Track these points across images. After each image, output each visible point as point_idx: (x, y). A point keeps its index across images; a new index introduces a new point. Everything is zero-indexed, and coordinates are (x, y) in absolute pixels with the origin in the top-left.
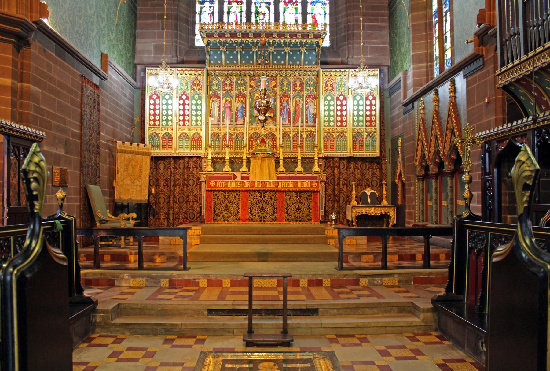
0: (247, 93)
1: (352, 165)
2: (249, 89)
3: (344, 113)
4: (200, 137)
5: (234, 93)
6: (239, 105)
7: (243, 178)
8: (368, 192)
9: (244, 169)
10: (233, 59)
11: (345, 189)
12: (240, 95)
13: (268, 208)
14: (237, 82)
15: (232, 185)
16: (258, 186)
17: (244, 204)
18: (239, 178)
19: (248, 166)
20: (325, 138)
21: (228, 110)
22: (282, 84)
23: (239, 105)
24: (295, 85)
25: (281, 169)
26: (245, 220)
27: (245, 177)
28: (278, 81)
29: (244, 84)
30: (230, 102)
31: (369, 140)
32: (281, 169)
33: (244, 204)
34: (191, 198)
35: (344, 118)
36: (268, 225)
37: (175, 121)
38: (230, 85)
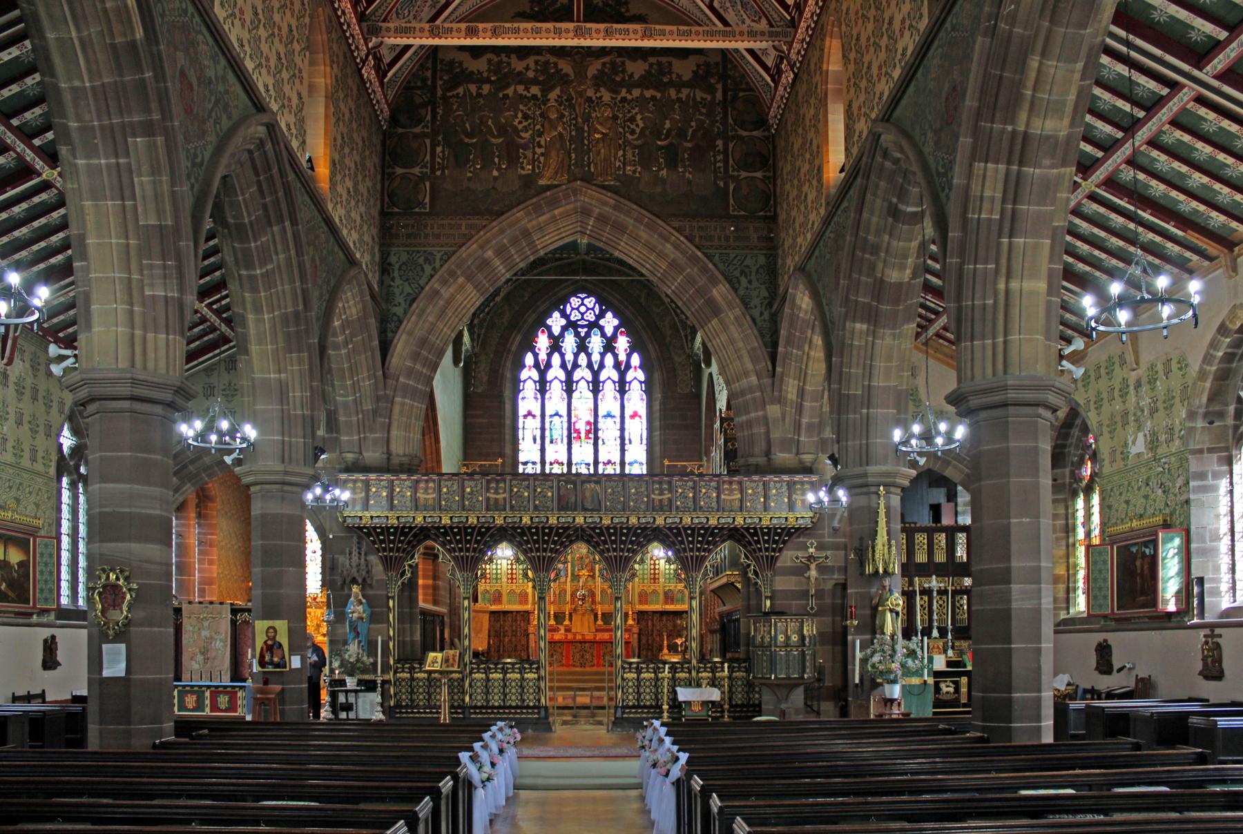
1: (664, 618)
4: (526, 594)
7: (566, 630)
8: (679, 641)
9: (567, 622)
13: (588, 656)
15: (557, 637)
16: (579, 637)
17: (568, 653)
18: (562, 631)
19: (571, 620)
20: (640, 594)
25: (600, 622)
26: (568, 666)
27: (568, 630)
31: (679, 596)
32: (600, 622)
33: (568, 653)
34: (519, 648)
36: (588, 669)
37: (504, 580)
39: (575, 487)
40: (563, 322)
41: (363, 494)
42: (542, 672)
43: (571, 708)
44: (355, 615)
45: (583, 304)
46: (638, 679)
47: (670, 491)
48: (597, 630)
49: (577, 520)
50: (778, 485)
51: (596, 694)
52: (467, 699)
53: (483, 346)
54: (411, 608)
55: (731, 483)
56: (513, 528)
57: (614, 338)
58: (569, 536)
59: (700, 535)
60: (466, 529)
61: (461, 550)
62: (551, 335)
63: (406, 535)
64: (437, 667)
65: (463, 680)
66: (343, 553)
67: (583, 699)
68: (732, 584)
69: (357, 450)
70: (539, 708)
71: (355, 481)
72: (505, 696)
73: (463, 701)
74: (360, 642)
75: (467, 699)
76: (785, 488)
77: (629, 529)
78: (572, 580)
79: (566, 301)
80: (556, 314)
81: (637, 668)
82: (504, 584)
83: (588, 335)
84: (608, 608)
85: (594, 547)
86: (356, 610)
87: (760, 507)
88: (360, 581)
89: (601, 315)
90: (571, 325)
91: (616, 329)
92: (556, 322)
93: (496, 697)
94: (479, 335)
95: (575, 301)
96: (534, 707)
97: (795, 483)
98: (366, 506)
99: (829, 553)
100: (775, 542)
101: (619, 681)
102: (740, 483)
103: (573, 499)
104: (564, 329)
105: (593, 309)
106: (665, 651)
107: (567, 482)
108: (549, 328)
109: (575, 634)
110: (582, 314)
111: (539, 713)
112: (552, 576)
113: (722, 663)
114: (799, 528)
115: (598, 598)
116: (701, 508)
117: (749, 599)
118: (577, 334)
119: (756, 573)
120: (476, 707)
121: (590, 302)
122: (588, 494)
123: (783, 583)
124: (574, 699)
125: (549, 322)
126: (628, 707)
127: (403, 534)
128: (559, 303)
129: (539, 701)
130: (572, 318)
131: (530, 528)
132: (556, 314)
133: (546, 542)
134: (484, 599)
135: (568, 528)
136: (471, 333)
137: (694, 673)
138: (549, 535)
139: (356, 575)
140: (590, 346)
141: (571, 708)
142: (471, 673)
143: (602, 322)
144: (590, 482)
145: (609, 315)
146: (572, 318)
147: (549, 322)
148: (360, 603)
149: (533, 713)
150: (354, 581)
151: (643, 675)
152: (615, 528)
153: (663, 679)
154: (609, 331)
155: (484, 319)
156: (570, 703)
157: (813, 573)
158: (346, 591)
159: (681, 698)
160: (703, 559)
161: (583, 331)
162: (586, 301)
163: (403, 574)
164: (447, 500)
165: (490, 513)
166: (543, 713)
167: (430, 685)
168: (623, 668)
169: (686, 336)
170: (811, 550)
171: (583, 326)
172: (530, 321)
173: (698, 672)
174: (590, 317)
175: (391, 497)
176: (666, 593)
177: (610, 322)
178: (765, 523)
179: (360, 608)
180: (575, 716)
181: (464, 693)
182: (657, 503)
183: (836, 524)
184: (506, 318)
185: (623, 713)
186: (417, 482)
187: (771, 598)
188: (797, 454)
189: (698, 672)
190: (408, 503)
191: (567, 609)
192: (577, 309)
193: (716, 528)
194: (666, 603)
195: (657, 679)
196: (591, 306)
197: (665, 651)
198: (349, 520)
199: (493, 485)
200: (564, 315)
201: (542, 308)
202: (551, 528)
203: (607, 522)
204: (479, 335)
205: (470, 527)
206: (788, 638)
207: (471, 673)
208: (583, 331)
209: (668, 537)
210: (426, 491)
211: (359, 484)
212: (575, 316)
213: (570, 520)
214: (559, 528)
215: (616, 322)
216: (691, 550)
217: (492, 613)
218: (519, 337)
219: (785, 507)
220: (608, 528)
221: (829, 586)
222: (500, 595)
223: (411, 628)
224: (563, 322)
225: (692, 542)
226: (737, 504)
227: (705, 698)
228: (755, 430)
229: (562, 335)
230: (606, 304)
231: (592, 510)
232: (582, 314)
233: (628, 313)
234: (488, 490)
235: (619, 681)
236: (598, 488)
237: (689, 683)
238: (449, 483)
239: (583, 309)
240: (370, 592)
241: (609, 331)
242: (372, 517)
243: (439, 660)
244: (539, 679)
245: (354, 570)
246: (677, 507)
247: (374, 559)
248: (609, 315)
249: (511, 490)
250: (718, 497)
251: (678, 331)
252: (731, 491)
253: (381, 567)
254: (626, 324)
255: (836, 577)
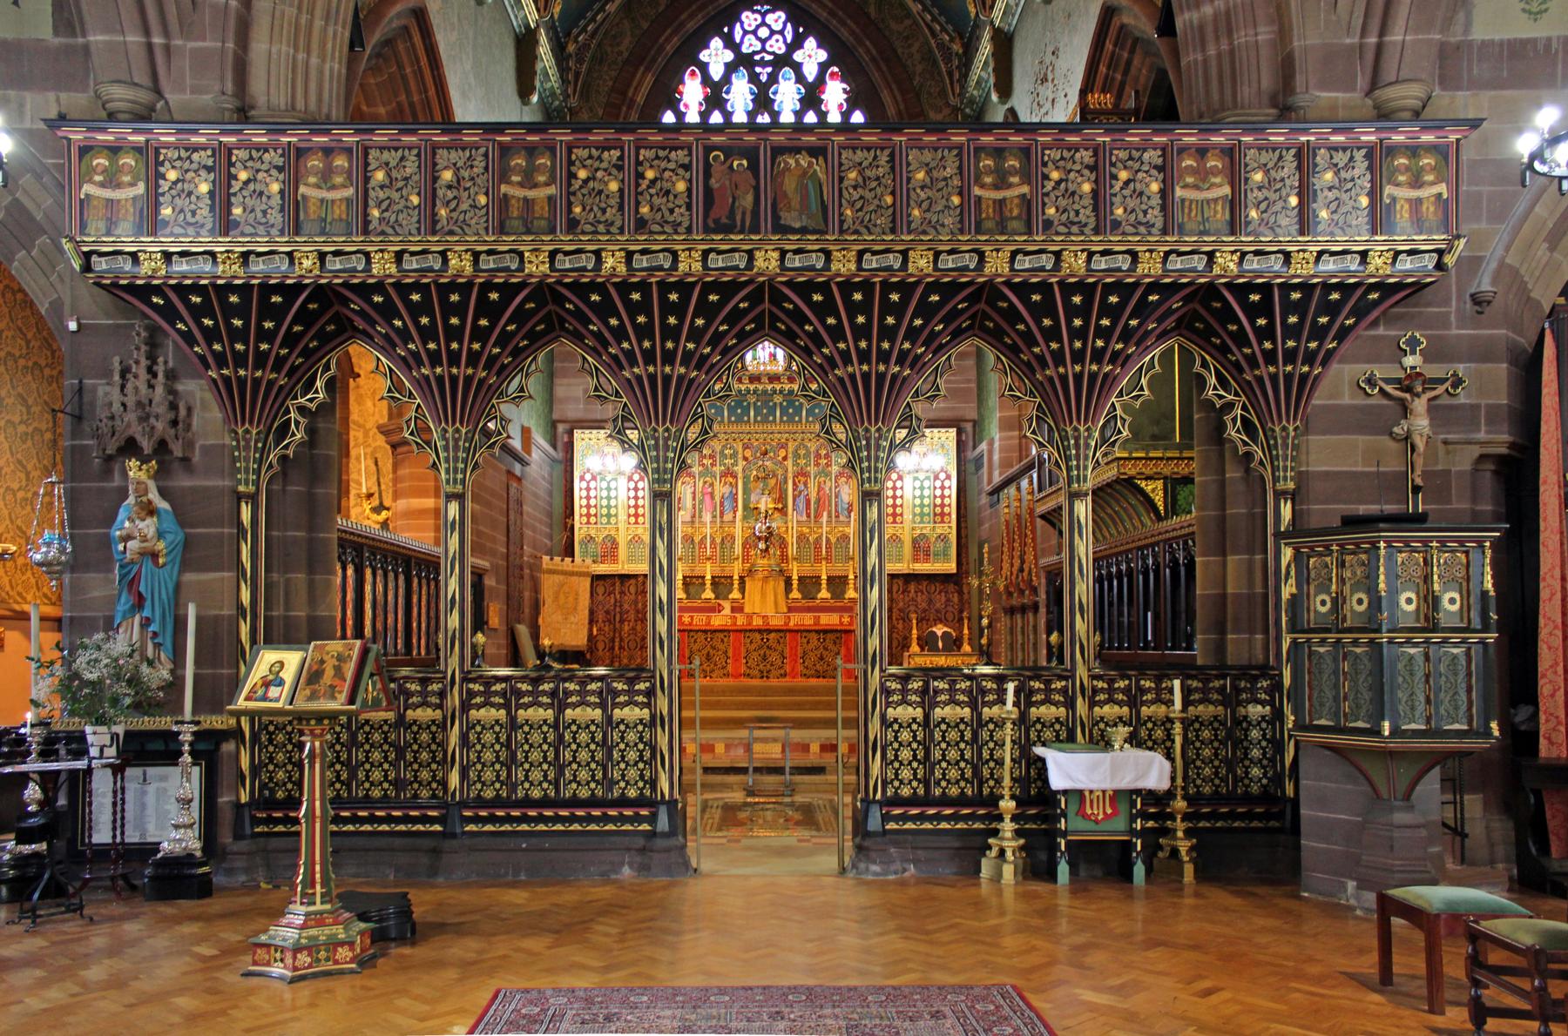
0: (739, 469)
1: (912, 587)
2: (741, 463)
3: (899, 502)
5: (718, 469)
6: (727, 490)
7: (733, 610)
9: (735, 595)
10: (767, 416)
11: (900, 626)
12: (729, 473)
13: (774, 657)
14: (722, 452)
15: (717, 621)
18: (727, 611)
19: (742, 590)
21: (708, 498)
22: (797, 456)
23: (727, 490)
24: (818, 456)
25: (795, 594)
27: (737, 608)
28: (790, 450)
29: (734, 455)
30: (712, 485)
31: (940, 545)
32: (795, 594)
35: (898, 510)
37: (622, 517)
38: (711, 457)
39: (754, 167)
40: (729, 56)
41: (140, 188)
42: (662, 704)
43: (744, 771)
44: (133, 545)
45: (764, 24)
46: (926, 721)
47: (1026, 178)
48: (790, 609)
49: (760, 263)
50: (1341, 158)
51: (797, 735)
52: (454, 779)
53: (585, 94)
54: (311, 528)
55: (1202, 152)
56: (575, 287)
57: (820, 81)
58: (735, 317)
59: (1106, 309)
60: (445, 290)
61: (435, 359)
62: (706, 80)
63: (277, 313)
64: (279, 698)
65: (443, 726)
66: (106, 374)
67: (769, 749)
68: (1129, 483)
69: (142, 77)
70: (652, 803)
71: (114, 150)
72: (560, 771)
73: (444, 784)
74: (146, 623)
75: (454, 779)
76: (1361, 165)
77: (906, 288)
78: (745, 518)
79: (733, 17)
80: (716, 43)
81: (924, 692)
82: (622, 526)
83: (773, 78)
84: (807, 570)
85: (807, 353)
86: (137, 529)
87: (1288, 222)
88: (147, 445)
89: (798, 43)
90: (743, 61)
91: (823, 67)
92: (716, 56)
93: (536, 775)
94: (577, 74)
95: (749, 19)
96: (639, 802)
97: (1392, 151)
98: (151, 222)
99: (1461, 369)
100: (1319, 333)
101: (875, 726)
102: (1231, 154)
103: (748, 201)
104: (730, 68)
105: (781, 32)
106: (915, 648)
107: (729, 152)
108: (704, 67)
109: (750, 617)
110: (763, 42)
111: (652, 819)
112: (693, 434)
113: (1000, 679)
114: (1399, 286)
115: (792, 550)
116: (1116, 225)
117: (1222, 503)
118: (754, 78)
119: (1248, 426)
120: (480, 802)
121: (777, 19)
122: (790, 184)
123: (1331, 454)
124: (748, 748)
125: (704, 56)
126: (897, 801)
127: (267, 311)
128: (721, 21)
129: (653, 783)
130: (745, 49)
131: (624, 287)
132: (716, 43)
133: (672, 333)
134: (585, 553)
135: (735, 286)
136: (559, 50)
137: (1081, 706)
138: (679, 310)
139: (136, 431)
140: (778, 98)
141: (744, 771)
142: (466, 706)
143: (798, 56)
144: (796, 150)
145: (811, 43)
146: (745, 49)
147: (704, 56)
148: (150, 510)
149: (638, 819)
150: (130, 448)
151: (938, 712)
152: (866, 287)
153: (1000, 724)
154: (810, 72)
155: (586, 46)
156: (738, 757)
157: (1421, 423)
158: (117, 481)
159: (1057, 782)
160: (1109, 381)
161: (764, 73)
162: (770, 18)
163: (284, 430)
164: (387, 206)
165: (507, 242)
166: (663, 823)
167: (353, 742)
168: (888, 692)
169: (950, 74)
170: (1410, 361)
171: (763, 63)
172: (669, 48)
173: (1092, 704)
174: (777, 46)
175: (222, 201)
176: (915, 542)
177: (812, 56)
178: (1302, 269)
179: (148, 526)
180: (750, 793)
181: (446, 763)
182: (988, 211)
183: (1485, 285)
184: (626, 43)
185: (886, 818)
186: (301, 153)
187: (1294, 496)
188: (1374, 85)
189: (1092, 704)
190: (275, 217)
191: (736, 569)
192: (754, 32)
193: (1155, 287)
194: (916, 560)
195: (979, 723)
196: (777, 27)
197: (915, 648)
198: (101, 265)
199: (519, 161)
200: (730, 43)
201: (691, 26)
202: (684, 287)
203: (844, 265)
204: (577, 74)
205: (453, 286)
206: (1431, 601)
207: (466, 706)
208: (764, 73)
209: (1013, 316)
210: (326, 176)
211: (128, 160)
212: (750, 45)
213: (739, 260)
214: (708, 288)
215: (822, 55)
216: (1078, 357)
217: (597, 579)
218: (649, 80)
219: (1362, 220)
220: (847, 286)
221: (1463, 461)
222: (615, 544)
223: (311, 585)
224: (729, 56)
225: (1081, 334)
226: (1221, 214)
227: (1126, 782)
228: (1241, 38)
229: (726, 79)
230: (805, 22)
231: (804, 231)
232: (763, 42)
233: (844, 34)
234: (504, 178)
235: (875, 726)
236: (818, 168)
237: (1066, 737)
238: (392, 157)
239: (763, 32)
240: (183, 482)
241: (810, 72)
242: (167, 256)
243: (288, 675)
244: (652, 723)
245: (131, 417)
246: (1048, 224)
247: (195, 389)
248: (811, 43)
249: (572, 176)
250: (1164, 193)
251: (935, 62)
252: (1203, 175)
253: (216, 414)
254: (841, 57)
255: (1482, 435)
